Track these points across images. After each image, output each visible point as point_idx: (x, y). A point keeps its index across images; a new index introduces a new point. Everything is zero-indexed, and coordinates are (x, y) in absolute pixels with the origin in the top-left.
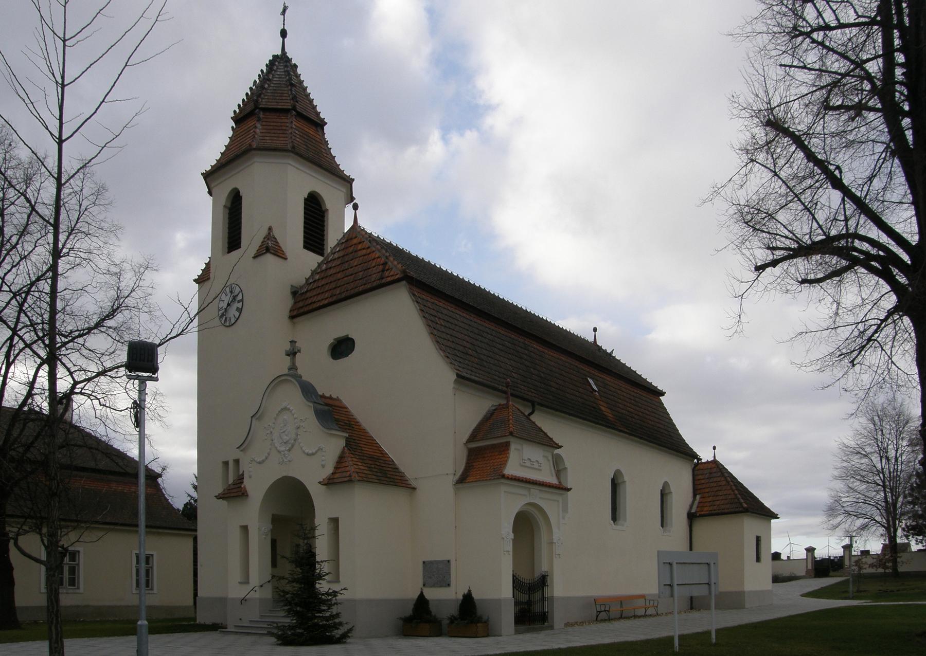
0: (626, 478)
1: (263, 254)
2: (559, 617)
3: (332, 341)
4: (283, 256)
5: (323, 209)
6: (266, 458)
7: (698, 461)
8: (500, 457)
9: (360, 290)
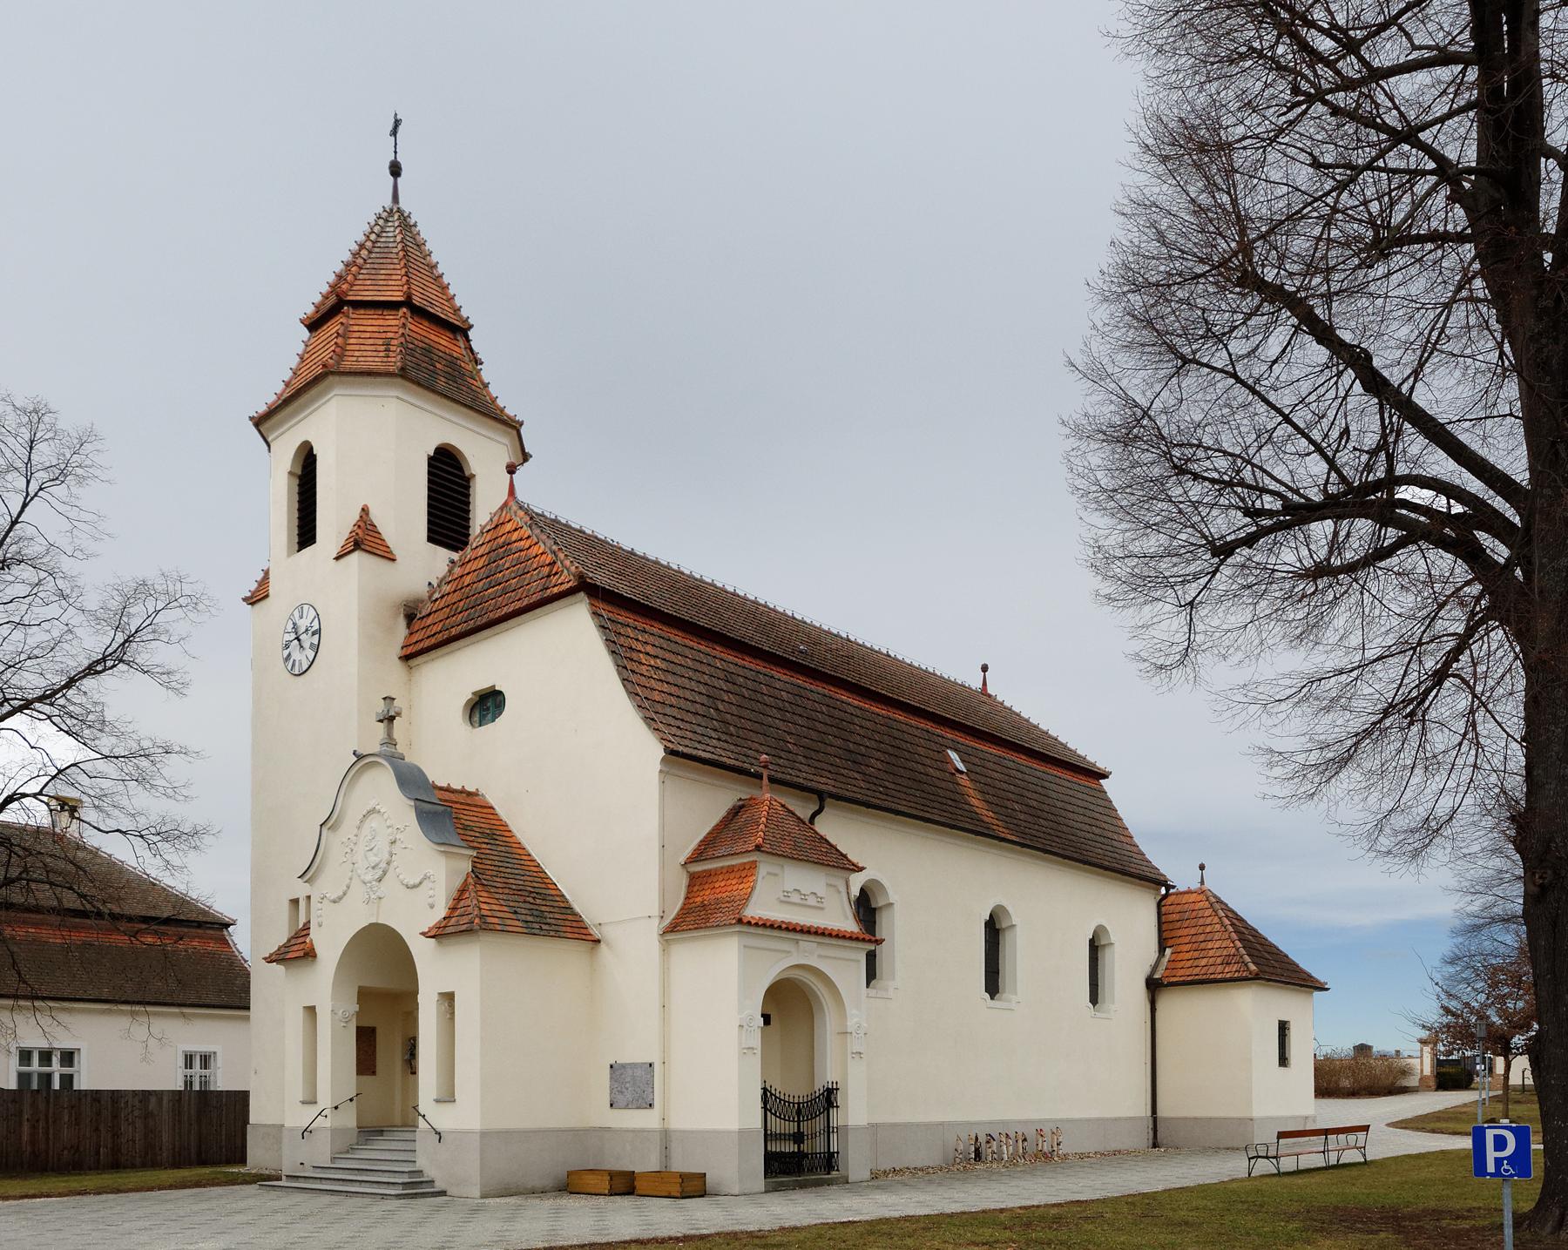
0: (1015, 920)
1: (349, 553)
2: (856, 1162)
3: (470, 696)
4: (389, 556)
5: (467, 474)
6: (345, 894)
7: (1167, 890)
8: (741, 887)
9: (511, 610)
